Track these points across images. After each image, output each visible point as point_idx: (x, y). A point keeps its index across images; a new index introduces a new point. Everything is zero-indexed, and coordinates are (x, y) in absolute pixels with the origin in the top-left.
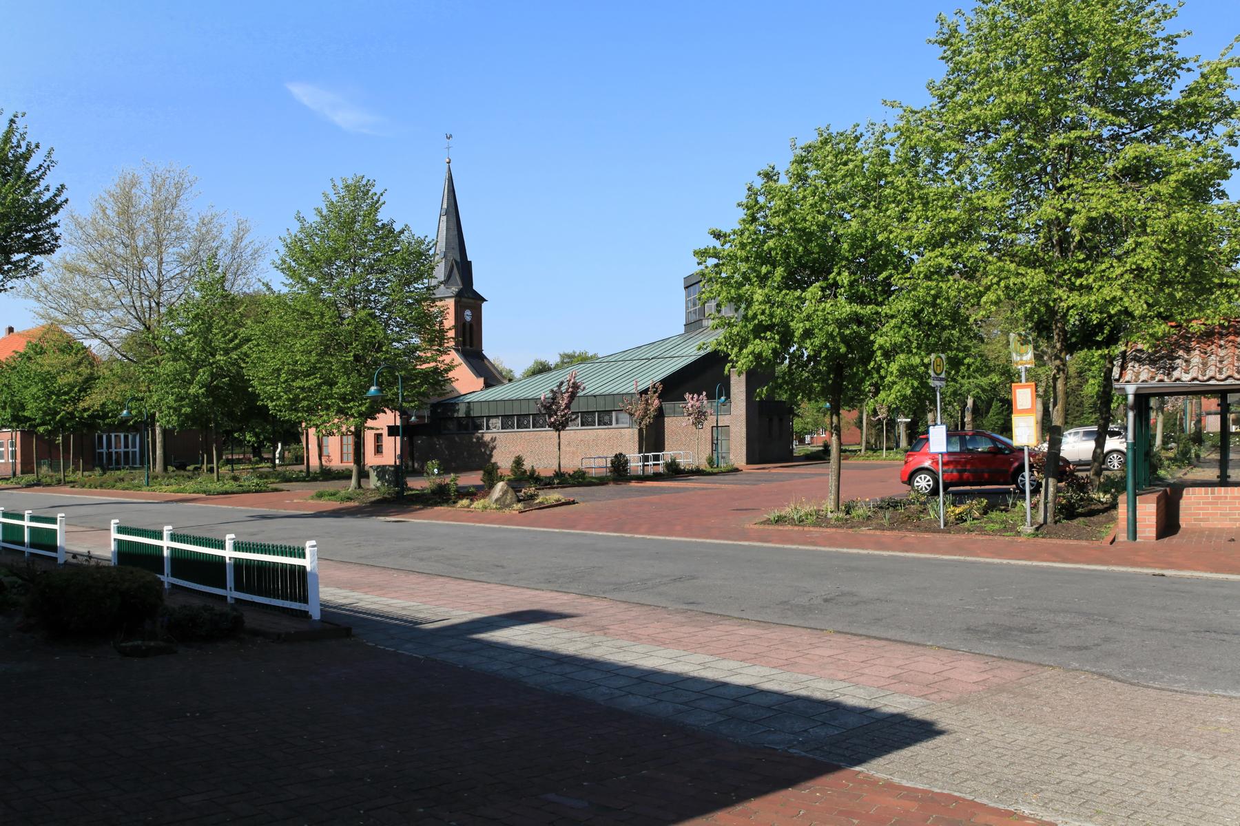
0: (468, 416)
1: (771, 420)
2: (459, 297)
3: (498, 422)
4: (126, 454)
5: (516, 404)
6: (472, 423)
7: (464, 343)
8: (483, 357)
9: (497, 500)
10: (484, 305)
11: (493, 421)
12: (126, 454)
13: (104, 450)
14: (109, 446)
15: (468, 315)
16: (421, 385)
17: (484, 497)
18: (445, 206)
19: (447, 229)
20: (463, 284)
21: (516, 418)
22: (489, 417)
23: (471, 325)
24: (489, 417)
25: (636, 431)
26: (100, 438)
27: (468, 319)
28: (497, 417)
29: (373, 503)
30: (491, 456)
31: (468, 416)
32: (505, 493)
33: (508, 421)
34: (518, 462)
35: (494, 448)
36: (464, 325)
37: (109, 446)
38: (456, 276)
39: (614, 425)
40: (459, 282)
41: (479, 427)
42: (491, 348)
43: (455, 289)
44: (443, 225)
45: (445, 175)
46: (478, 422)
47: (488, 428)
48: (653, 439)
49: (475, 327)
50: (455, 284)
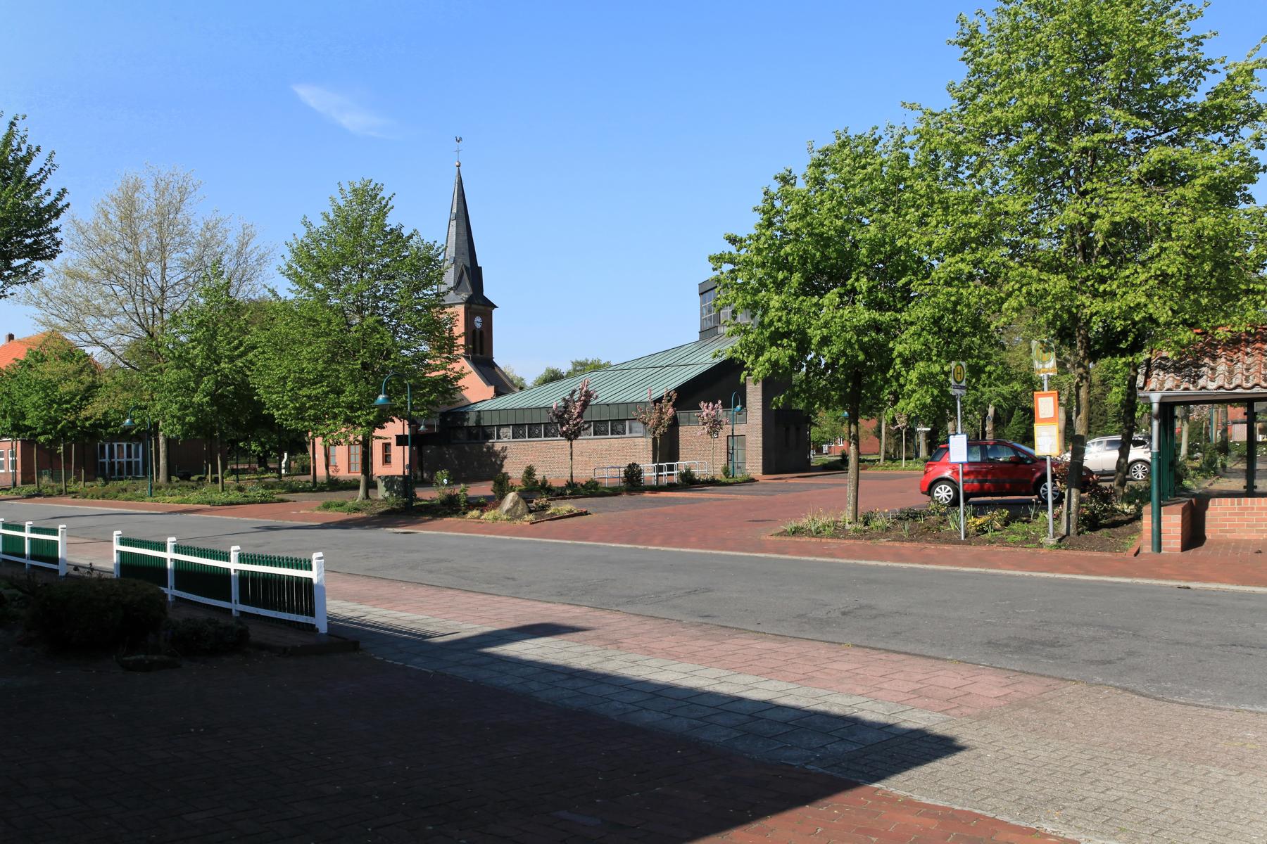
0: (478, 425)
1: (787, 429)
2: (469, 303)
3: (509, 431)
4: (129, 463)
5: (527, 413)
6: (482, 433)
7: (474, 351)
8: (493, 365)
9: (507, 511)
10: (495, 312)
11: (503, 430)
12: (129, 463)
13: (107, 460)
14: (111, 456)
15: (478, 322)
16: (430, 393)
17: (494, 508)
18: (455, 210)
19: (457, 234)
20: (473, 290)
21: (527, 427)
22: (500, 427)
23: (481, 332)
24: (500, 427)
25: (650, 441)
26: (103, 447)
27: (479, 326)
28: (508, 426)
29: (381, 514)
30: (502, 466)
31: (478, 425)
32: (516, 504)
33: (519, 430)
34: (530, 472)
35: (505, 457)
36: (474, 332)
37: (111, 456)
38: (466, 282)
39: (627, 434)
40: (469, 289)
41: (490, 436)
42: (502, 356)
43: (465, 296)
44: (453, 230)
45: (455, 179)
46: (488, 431)
47: (499, 437)
48: (667, 448)
49: (485, 334)
50: (465, 290)
